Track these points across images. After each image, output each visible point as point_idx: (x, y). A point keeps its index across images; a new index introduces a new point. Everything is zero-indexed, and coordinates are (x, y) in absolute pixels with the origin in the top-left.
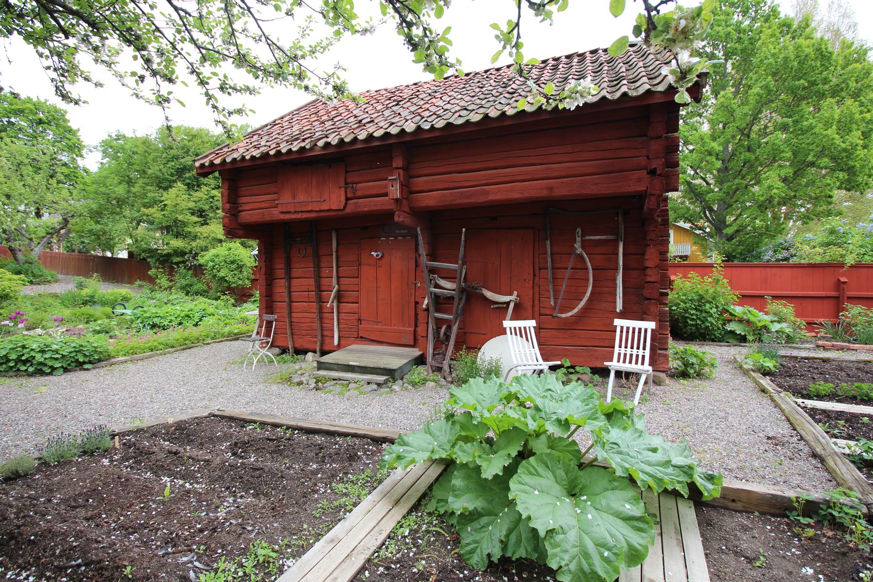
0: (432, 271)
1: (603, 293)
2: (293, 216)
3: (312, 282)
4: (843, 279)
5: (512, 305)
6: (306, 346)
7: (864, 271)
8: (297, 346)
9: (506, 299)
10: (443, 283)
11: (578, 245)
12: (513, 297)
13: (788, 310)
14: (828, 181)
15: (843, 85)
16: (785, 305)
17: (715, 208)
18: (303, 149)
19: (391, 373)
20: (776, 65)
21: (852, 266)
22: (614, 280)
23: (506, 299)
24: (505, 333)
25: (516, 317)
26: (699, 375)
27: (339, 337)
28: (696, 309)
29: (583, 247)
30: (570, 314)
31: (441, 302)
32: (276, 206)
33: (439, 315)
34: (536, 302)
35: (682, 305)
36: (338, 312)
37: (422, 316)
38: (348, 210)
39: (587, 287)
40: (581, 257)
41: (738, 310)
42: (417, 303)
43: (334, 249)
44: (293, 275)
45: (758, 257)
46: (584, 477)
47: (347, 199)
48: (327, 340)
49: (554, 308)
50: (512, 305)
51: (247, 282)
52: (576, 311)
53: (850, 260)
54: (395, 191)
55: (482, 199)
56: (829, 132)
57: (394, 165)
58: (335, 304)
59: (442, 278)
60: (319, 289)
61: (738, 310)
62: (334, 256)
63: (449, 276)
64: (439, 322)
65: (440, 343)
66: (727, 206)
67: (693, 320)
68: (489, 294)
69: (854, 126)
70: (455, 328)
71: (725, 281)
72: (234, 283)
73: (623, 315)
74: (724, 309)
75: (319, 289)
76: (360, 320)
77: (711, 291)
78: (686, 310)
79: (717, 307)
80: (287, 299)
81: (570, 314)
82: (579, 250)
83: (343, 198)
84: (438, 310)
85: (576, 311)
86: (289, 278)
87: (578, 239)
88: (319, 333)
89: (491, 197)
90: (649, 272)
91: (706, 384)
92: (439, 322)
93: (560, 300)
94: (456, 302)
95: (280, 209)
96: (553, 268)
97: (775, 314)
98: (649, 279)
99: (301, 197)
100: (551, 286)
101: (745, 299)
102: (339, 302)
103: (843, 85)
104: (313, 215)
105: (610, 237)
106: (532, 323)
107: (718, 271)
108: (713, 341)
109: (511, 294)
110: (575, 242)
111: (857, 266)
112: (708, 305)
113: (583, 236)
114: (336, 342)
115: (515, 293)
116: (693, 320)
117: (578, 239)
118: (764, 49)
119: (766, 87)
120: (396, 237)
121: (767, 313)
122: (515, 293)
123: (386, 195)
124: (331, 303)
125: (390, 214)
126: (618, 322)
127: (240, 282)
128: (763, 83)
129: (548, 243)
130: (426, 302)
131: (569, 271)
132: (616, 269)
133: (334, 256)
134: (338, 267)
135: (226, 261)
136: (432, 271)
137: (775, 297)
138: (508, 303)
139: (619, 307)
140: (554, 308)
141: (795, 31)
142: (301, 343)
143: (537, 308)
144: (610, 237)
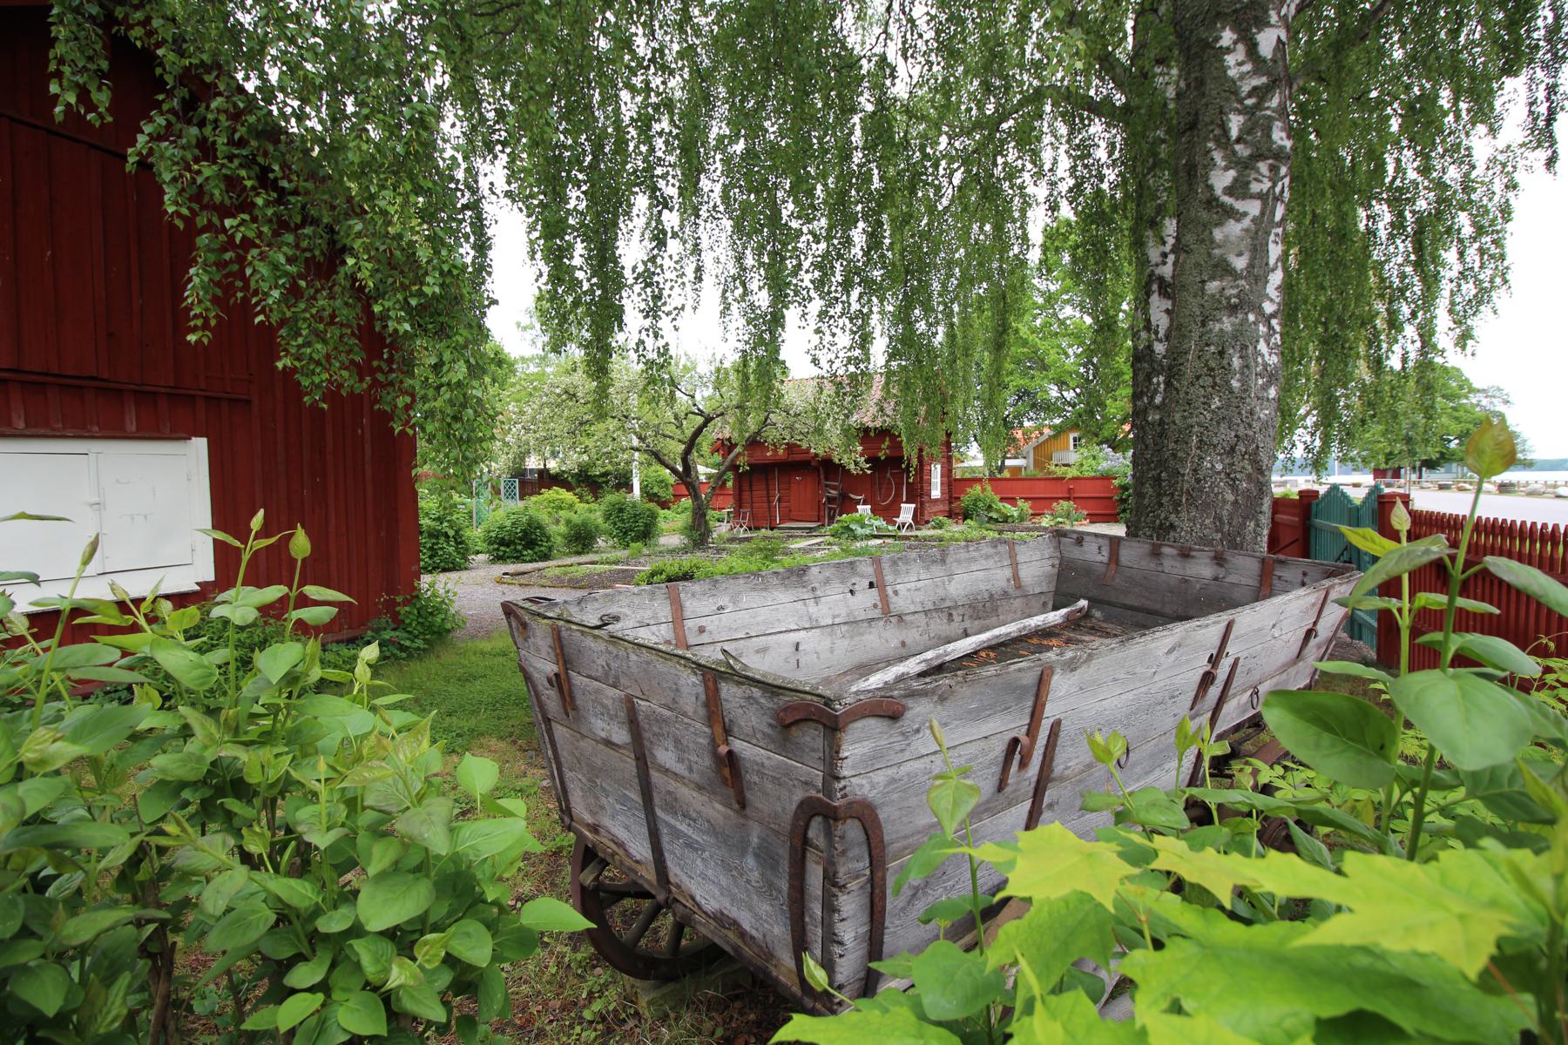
31: (831, 500)
41: (1000, 505)
60: (768, 496)
63: (834, 488)
64: (830, 509)
75: (768, 496)
101: (1002, 500)
111: (1074, 479)
124: (775, 503)
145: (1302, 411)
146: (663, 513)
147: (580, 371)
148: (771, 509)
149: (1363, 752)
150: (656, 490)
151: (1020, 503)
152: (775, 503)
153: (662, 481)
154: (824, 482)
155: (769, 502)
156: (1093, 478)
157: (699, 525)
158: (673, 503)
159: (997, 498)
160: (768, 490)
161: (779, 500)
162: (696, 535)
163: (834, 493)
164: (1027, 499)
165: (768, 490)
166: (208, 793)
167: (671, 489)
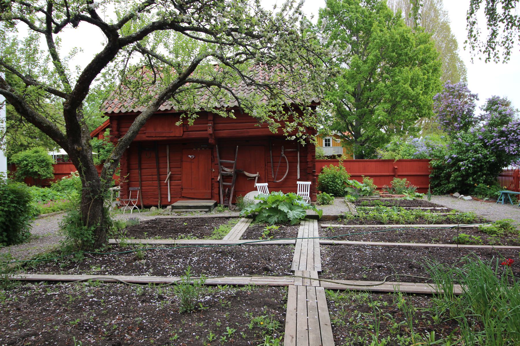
0: (222, 164)
1: (293, 172)
2: (154, 139)
3: (155, 170)
4: (396, 167)
5: (257, 178)
6: (150, 204)
7: (404, 163)
8: (145, 204)
9: (254, 175)
10: (226, 169)
11: (282, 153)
12: (257, 175)
13: (371, 181)
14: (407, 113)
15: (415, 57)
16: (369, 179)
17: (354, 124)
18: (166, 110)
19: (209, 207)
20: (381, 43)
21: (397, 161)
22: (297, 166)
23: (254, 175)
24: (257, 190)
25: (259, 182)
26: (328, 204)
27: (171, 198)
28: (332, 182)
29: (284, 153)
30: (280, 181)
31: (226, 178)
32: (145, 133)
33: (224, 183)
34: (266, 177)
35: (326, 180)
36: (170, 185)
37: (216, 185)
38: (184, 137)
39: (286, 170)
40: (284, 157)
41: (351, 182)
42: (212, 179)
43: (168, 154)
44: (142, 167)
45: (376, 156)
46: (293, 207)
47: (184, 132)
48: (163, 200)
49: (274, 179)
50: (257, 178)
51: (53, 175)
52: (282, 179)
53: (397, 158)
54: (210, 131)
55: (246, 135)
56: (406, 86)
57: (209, 119)
58: (169, 182)
59: (226, 167)
60: (159, 174)
61: (351, 182)
62: (168, 157)
63: (229, 166)
64: (225, 187)
65: (227, 196)
66: (360, 123)
67: (331, 187)
68: (247, 174)
69: (419, 82)
70: (233, 189)
71: (344, 168)
72: (44, 176)
73: (300, 180)
74: (344, 181)
75: (159, 174)
76: (182, 189)
77: (338, 173)
78: (328, 183)
79: (341, 180)
80: (140, 180)
81: (280, 181)
82: (283, 155)
83: (182, 132)
84: (224, 182)
85: (282, 179)
86: (140, 168)
87: (283, 150)
88: (159, 196)
89: (250, 134)
90: (308, 163)
91: (330, 206)
92: (225, 187)
93: (277, 174)
94: (233, 178)
95: (147, 135)
96: (273, 162)
97: (365, 183)
98: (309, 166)
99: (159, 130)
100: (272, 169)
101: (352, 177)
102: (170, 180)
103: (415, 57)
104: (165, 138)
105: (295, 150)
106: (266, 184)
107: (341, 164)
108: (340, 196)
109: (256, 173)
110: (281, 151)
111: (399, 161)
112: (337, 180)
113: (284, 149)
114: (169, 200)
115: (258, 173)
116: (331, 187)
117: (283, 150)
118: (375, 33)
119: (376, 56)
120: (201, 149)
121: (362, 183)
122: (258, 173)
123: (207, 130)
124: (167, 180)
125: (207, 139)
126: (298, 182)
127: (49, 176)
128: (375, 53)
129: (271, 152)
130: (219, 178)
131: (279, 163)
132: (297, 162)
133: (168, 157)
134: (169, 163)
135: (36, 161)
136: (222, 164)
137: (365, 176)
138: (255, 177)
139: (299, 177)
140: (274, 179)
141: (394, 19)
142: (147, 202)
143: (267, 179)
144: (295, 150)
145: (481, 124)
146: (34, 191)
147: (4, 122)
148: (161, 187)
149: (55, 214)
150: (36, 169)
151: (366, 180)
152: (167, 180)
153: (42, 161)
154: (219, 160)
155: (160, 180)
156: (412, 161)
157: (94, 217)
158: (54, 181)
159: (348, 175)
160: (158, 168)
161: (171, 178)
162: (89, 234)
163: (228, 171)
164: (371, 176)
165: (158, 168)
166: (52, 145)
167: (52, 168)
